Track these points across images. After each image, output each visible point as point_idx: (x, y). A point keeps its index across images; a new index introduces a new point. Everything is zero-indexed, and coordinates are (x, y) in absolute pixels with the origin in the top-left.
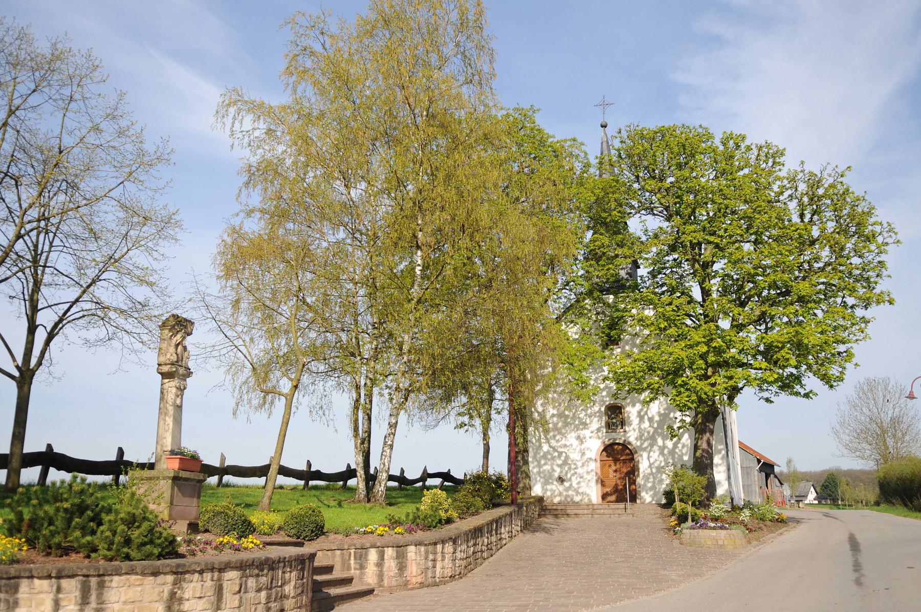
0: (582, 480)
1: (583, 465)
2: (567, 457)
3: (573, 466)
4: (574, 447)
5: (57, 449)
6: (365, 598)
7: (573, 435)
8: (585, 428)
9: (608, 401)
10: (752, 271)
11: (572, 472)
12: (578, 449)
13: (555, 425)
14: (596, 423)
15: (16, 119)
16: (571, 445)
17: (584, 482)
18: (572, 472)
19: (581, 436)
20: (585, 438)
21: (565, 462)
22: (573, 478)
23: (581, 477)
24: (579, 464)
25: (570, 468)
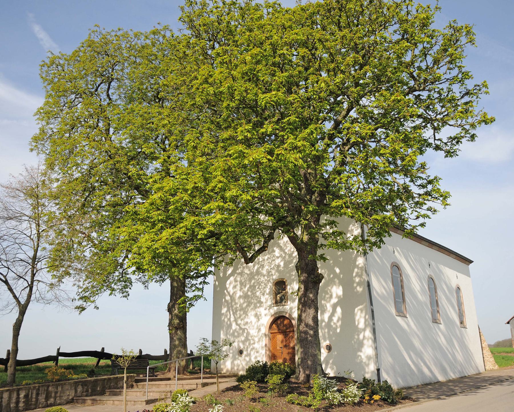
0: (258, 354)
1: (259, 341)
2: (248, 334)
3: (252, 342)
4: (253, 323)
5: (106, 351)
6: (464, 312)
7: (253, 313)
8: (260, 306)
9: (276, 276)
10: (293, 101)
11: (251, 347)
12: (256, 326)
13: (241, 305)
14: (267, 299)
15: (22, 256)
16: (251, 322)
17: (260, 356)
18: (251, 347)
19: (258, 313)
20: (261, 315)
21: (247, 339)
22: (252, 353)
23: (257, 352)
24: (256, 339)
25: (250, 344)
